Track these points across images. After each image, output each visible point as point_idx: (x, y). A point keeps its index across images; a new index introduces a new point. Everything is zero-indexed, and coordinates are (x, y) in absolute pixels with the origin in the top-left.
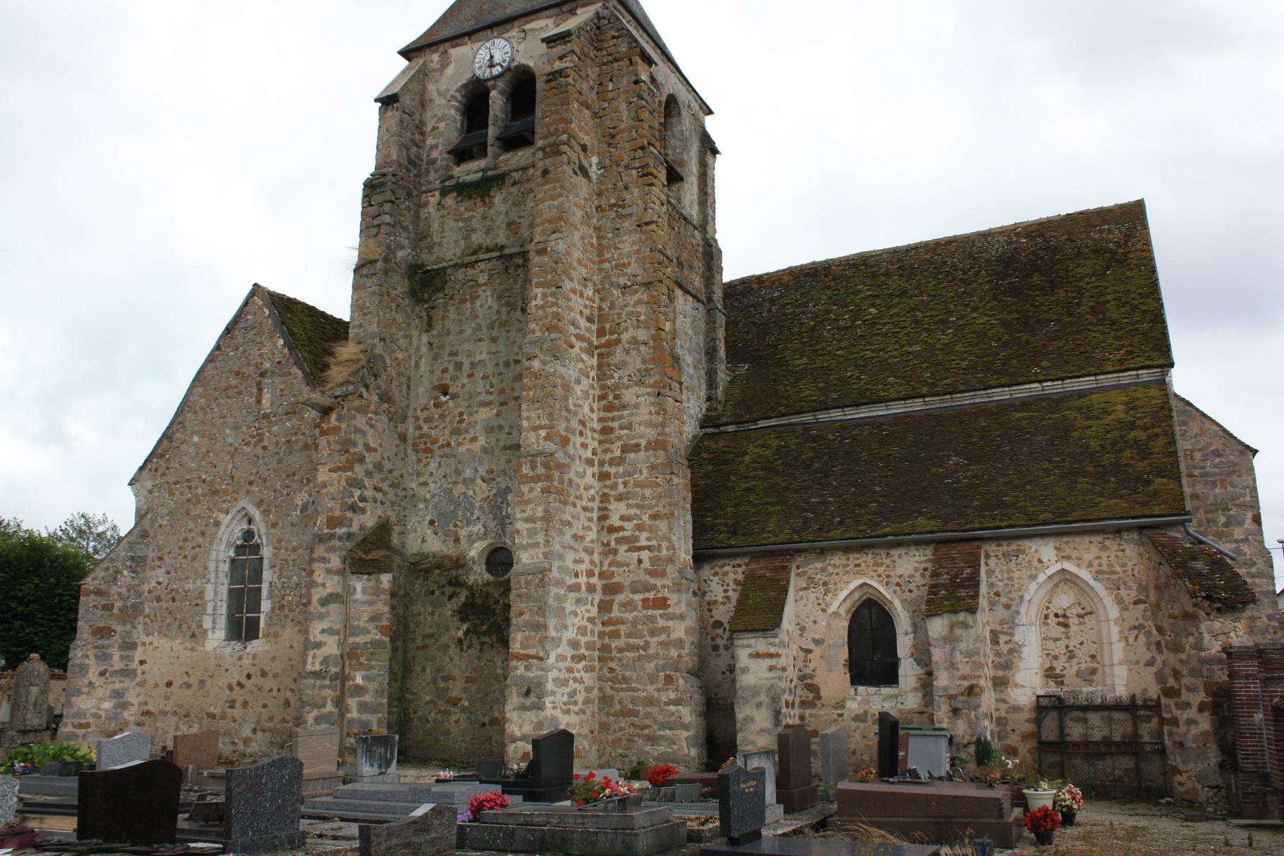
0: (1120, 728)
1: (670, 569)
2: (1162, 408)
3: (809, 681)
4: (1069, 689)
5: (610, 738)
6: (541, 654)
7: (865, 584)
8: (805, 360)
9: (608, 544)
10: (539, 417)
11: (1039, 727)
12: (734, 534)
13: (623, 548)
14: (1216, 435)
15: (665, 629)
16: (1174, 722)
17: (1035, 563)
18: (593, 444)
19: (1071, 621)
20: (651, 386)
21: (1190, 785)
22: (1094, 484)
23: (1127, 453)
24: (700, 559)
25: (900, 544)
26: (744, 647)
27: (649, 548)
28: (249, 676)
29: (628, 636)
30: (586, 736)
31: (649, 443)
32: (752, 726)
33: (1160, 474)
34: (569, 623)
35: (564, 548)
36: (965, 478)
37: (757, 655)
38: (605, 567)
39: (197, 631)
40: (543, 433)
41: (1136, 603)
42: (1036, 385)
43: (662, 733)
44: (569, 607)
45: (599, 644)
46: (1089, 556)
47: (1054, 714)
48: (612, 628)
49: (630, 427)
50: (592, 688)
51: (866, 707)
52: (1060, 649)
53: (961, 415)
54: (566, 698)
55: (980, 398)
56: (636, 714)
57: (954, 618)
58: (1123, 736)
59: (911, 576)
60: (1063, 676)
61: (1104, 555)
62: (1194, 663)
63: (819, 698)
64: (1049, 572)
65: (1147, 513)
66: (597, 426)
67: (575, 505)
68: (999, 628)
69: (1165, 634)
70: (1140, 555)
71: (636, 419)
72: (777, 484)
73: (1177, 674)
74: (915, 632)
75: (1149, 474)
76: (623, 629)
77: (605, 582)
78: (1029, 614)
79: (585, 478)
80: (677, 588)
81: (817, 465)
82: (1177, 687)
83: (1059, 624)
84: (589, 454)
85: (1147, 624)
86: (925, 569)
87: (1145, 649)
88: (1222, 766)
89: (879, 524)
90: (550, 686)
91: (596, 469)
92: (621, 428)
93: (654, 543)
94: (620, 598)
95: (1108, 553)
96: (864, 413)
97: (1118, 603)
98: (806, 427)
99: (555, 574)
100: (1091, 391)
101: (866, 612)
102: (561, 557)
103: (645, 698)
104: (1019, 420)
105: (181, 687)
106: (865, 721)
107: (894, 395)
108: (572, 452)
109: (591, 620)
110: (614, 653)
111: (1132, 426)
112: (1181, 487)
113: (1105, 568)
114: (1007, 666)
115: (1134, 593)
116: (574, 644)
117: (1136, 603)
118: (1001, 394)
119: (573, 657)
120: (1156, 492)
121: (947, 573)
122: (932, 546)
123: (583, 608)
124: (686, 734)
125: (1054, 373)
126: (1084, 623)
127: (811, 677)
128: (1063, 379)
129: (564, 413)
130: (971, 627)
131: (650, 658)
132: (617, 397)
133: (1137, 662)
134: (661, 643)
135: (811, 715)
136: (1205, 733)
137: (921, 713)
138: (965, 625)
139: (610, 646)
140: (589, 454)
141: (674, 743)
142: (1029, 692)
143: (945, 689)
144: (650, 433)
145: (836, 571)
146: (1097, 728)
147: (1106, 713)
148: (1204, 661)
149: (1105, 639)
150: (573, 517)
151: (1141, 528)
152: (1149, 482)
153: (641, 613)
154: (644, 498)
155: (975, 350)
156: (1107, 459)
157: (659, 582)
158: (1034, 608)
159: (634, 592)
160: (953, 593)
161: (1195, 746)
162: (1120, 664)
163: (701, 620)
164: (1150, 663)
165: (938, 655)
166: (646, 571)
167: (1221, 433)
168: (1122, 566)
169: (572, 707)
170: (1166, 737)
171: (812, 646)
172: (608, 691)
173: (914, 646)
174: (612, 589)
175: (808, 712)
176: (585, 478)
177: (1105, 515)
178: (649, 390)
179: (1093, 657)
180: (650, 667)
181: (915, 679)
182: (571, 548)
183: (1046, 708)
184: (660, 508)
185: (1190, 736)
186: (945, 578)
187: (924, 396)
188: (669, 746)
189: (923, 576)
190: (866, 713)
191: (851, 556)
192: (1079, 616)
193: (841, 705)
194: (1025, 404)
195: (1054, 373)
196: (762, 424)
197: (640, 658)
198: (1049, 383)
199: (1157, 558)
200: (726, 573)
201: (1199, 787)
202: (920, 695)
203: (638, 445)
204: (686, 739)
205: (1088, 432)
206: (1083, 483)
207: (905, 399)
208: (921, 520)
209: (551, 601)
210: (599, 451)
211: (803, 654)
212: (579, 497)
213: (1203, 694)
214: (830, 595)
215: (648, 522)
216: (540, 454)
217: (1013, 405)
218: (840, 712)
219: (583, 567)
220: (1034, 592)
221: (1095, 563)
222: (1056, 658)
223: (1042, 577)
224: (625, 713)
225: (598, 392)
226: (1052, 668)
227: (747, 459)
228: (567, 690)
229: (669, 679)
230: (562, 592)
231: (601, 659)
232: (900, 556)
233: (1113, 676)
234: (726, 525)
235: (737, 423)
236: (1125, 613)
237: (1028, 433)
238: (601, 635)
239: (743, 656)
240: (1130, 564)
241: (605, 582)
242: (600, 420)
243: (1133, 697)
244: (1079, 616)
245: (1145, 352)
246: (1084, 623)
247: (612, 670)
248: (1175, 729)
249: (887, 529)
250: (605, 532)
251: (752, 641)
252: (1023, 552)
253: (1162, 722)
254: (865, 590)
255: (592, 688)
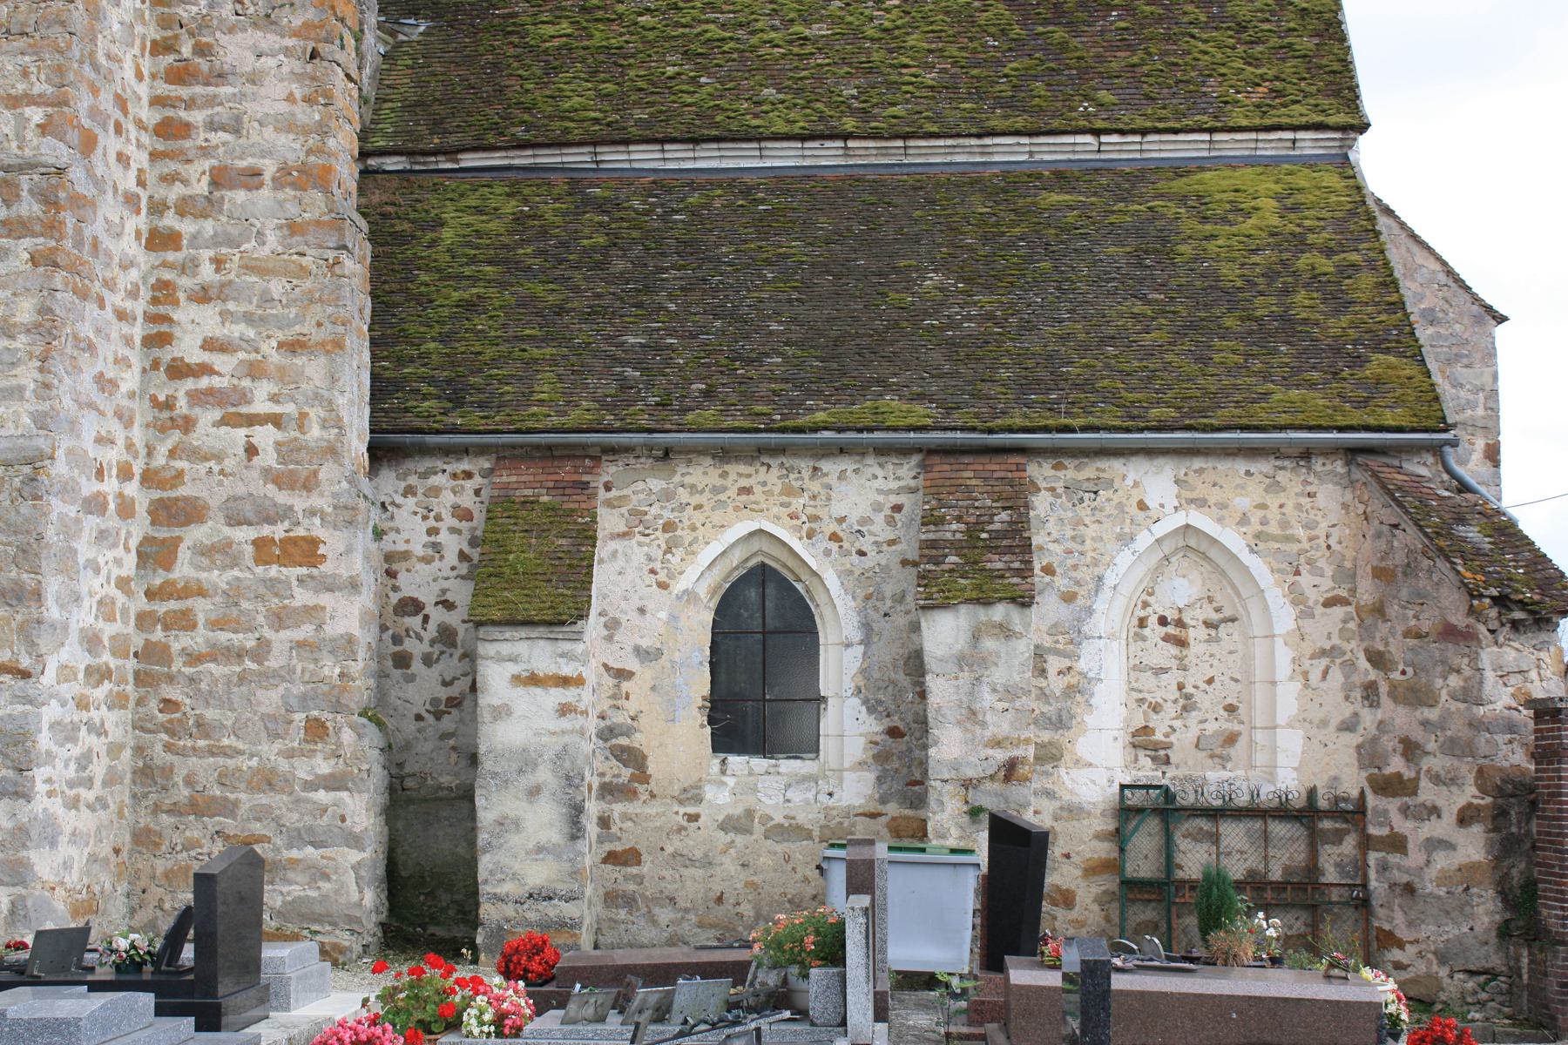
0: (1285, 852)
1: (328, 471)
2: (1352, 213)
3: (623, 741)
4: (1180, 773)
5: (161, 866)
6: (25, 662)
7: (761, 532)
8: (565, 27)
9: (169, 405)
10: (25, 74)
11: (1122, 850)
12: (457, 402)
13: (207, 417)
14: (1431, 281)
15: (312, 613)
16: (1397, 843)
17: (1134, 510)
18: (140, 159)
19: (1192, 633)
20: (296, 34)
21: (1420, 968)
22: (1248, 355)
23: (1301, 297)
24: (381, 453)
25: (842, 450)
26: (500, 659)
27: (276, 421)
29: (216, 625)
30: (106, 861)
31: (285, 170)
32: (514, 840)
33: (1379, 346)
34: (84, 590)
35: (81, 405)
36: (969, 318)
37: (533, 680)
38: (160, 460)
40: (36, 115)
41: (1328, 603)
42: (1088, 139)
43: (294, 854)
44: (84, 549)
45: (138, 642)
46: (1242, 503)
47: (1153, 824)
48: (173, 605)
49: (236, 128)
50: (121, 747)
51: (750, 801)
52: (1165, 687)
53: (928, 188)
54: (71, 772)
55: (963, 153)
56: (230, 808)
57: (982, 614)
58: (1286, 869)
59: (865, 521)
60: (1169, 746)
61: (1273, 501)
62: (1457, 729)
63: (644, 778)
64: (1160, 530)
65: (1372, 421)
66: (151, 116)
67: (101, 304)
68: (1047, 642)
69: (1389, 668)
70: (1345, 506)
71: (253, 108)
72: (534, 297)
73: (1410, 749)
74: (866, 642)
75: (1355, 343)
76: (201, 608)
77: (156, 494)
78: (1109, 614)
79: (118, 234)
80: (346, 517)
81: (619, 265)
82: (1408, 774)
83: (1167, 638)
84: (129, 183)
85: (1347, 647)
86: (897, 508)
87: (1341, 696)
88: (1504, 932)
89: (795, 404)
90: (44, 741)
91: (141, 221)
92: (212, 126)
93: (289, 408)
94: (196, 534)
95: (1282, 498)
96: (709, 159)
97: (1294, 603)
98: (576, 181)
99: (60, 468)
100: (1201, 165)
101: (753, 594)
102: (73, 426)
103: (255, 772)
104: (1056, 208)
105: (1356, 714)
106: (749, 832)
107: (780, 127)
108: (99, 171)
109: (123, 583)
110: (178, 665)
111: (1300, 243)
112: (1428, 374)
113: (1273, 528)
114: (1060, 722)
115: (1327, 583)
116: (92, 642)
117: (1328, 603)
118: (1010, 151)
119: (89, 671)
120: (1379, 381)
121: (959, 519)
122: (916, 459)
123: (110, 555)
124: (354, 856)
125: (1126, 118)
126: (1218, 640)
127: (628, 732)
128: (1144, 132)
129: (87, 68)
130: (1019, 636)
131: (269, 678)
132: (202, 50)
133: (1324, 723)
134: (301, 645)
135: (625, 817)
136: (1472, 867)
137: (873, 816)
138: (1005, 631)
139: (166, 648)
140: (129, 183)
141: (326, 877)
142: (1101, 776)
143: (955, 766)
144: (290, 147)
145: (695, 500)
146: (1239, 853)
147: (1258, 824)
148: (1476, 725)
149: (1259, 674)
150: (98, 331)
151: (1352, 453)
152: (1358, 361)
153: (252, 573)
154: (266, 299)
155: (952, 50)
156: (1264, 306)
157: (299, 502)
158: (1121, 603)
159: (235, 521)
160: (981, 561)
161: (1442, 892)
162: (1290, 726)
163: (382, 597)
164: (1348, 726)
165: (941, 691)
166: (267, 473)
167: (1442, 278)
168: (1306, 527)
169: (82, 792)
170: (1372, 874)
171: (632, 664)
172: (160, 756)
173: (863, 671)
174: (175, 513)
175: (618, 809)
176: (118, 234)
177: (1284, 419)
178: (290, 42)
179: (1231, 709)
180: (270, 699)
181: (861, 742)
182: (91, 405)
183: (1139, 811)
184: (308, 328)
185: (1433, 872)
186: (953, 530)
187: (846, 137)
188: (312, 883)
189: (890, 521)
190: (749, 813)
191: (734, 469)
192: (1208, 624)
193: (692, 794)
194: (1062, 177)
195: (1126, 118)
196: (470, 160)
197: (242, 678)
198: (1115, 138)
199: (1391, 514)
200: (435, 491)
201: (1443, 972)
202: (870, 776)
203: (256, 173)
204: (356, 868)
205: (1211, 246)
206: (1225, 352)
207: (803, 138)
208: (890, 401)
209: (51, 534)
210: (151, 178)
211: (611, 681)
212: (110, 285)
213: (1474, 790)
214: (679, 552)
215: (275, 358)
216: (27, 167)
217: (1039, 176)
218: (691, 810)
219: (112, 456)
220: (1124, 570)
221: (1255, 520)
222: (1156, 708)
223: (1144, 540)
224: (198, 807)
225: (154, 33)
226: (1146, 730)
227: (447, 234)
228: (76, 751)
229: (316, 730)
230: (72, 511)
231: (140, 679)
232: (842, 476)
233: (1274, 750)
234: (431, 381)
235: (410, 154)
236: (1307, 624)
237: (1084, 236)
238: (144, 621)
239: (496, 680)
240: (1324, 525)
241: (156, 494)
242: (157, 101)
243: (1312, 792)
244: (1208, 624)
245: (1307, 95)
246: (1218, 640)
247: (168, 705)
248: (1394, 859)
249: (820, 416)
250: (161, 375)
251: (522, 648)
252: (1110, 484)
253: (1366, 843)
254: (756, 545)
255: (121, 747)
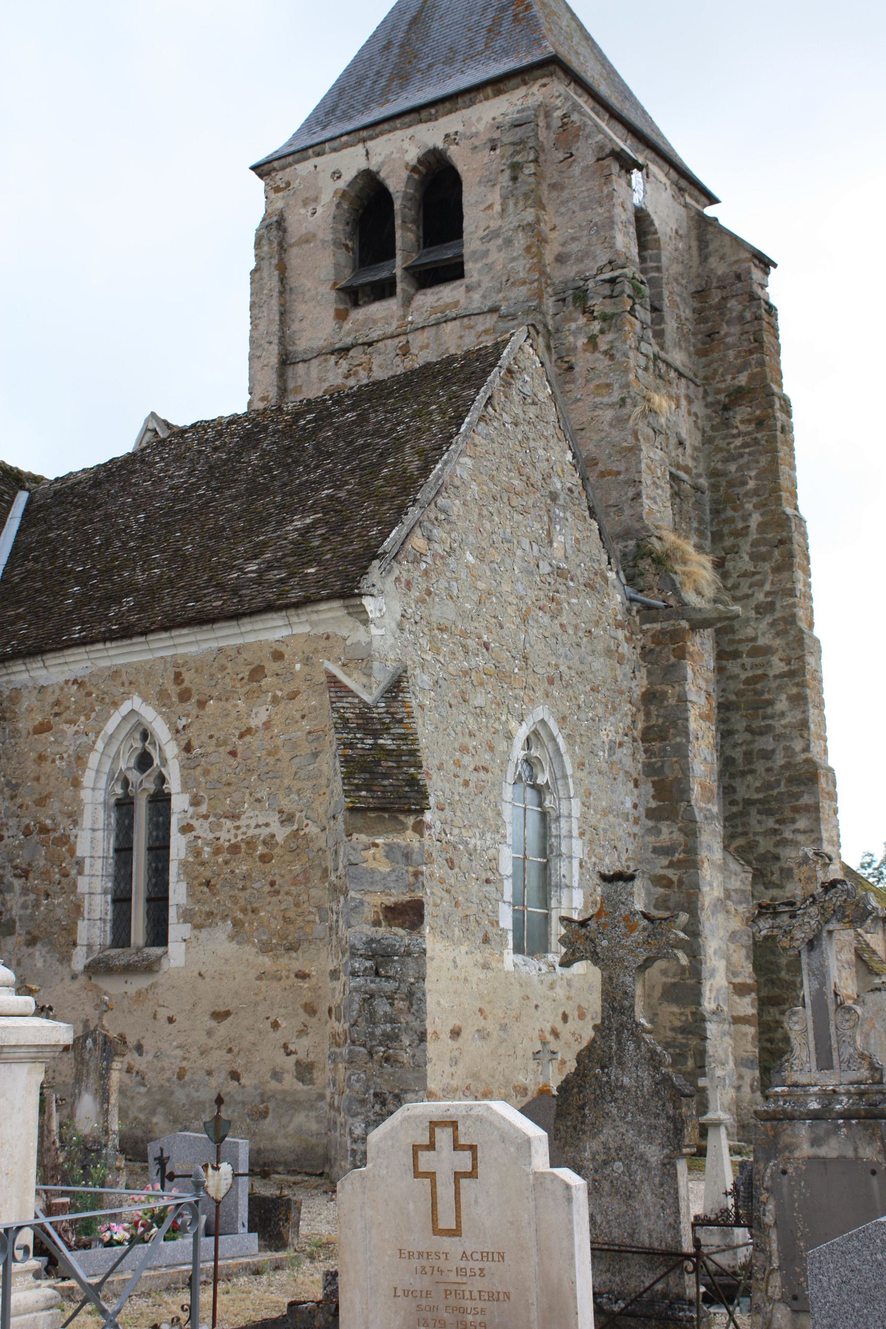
28: (565, 1018)
39: (492, 931)
